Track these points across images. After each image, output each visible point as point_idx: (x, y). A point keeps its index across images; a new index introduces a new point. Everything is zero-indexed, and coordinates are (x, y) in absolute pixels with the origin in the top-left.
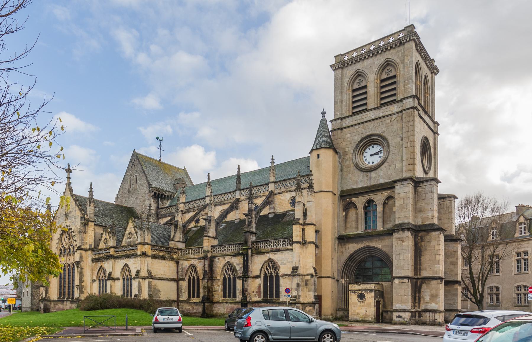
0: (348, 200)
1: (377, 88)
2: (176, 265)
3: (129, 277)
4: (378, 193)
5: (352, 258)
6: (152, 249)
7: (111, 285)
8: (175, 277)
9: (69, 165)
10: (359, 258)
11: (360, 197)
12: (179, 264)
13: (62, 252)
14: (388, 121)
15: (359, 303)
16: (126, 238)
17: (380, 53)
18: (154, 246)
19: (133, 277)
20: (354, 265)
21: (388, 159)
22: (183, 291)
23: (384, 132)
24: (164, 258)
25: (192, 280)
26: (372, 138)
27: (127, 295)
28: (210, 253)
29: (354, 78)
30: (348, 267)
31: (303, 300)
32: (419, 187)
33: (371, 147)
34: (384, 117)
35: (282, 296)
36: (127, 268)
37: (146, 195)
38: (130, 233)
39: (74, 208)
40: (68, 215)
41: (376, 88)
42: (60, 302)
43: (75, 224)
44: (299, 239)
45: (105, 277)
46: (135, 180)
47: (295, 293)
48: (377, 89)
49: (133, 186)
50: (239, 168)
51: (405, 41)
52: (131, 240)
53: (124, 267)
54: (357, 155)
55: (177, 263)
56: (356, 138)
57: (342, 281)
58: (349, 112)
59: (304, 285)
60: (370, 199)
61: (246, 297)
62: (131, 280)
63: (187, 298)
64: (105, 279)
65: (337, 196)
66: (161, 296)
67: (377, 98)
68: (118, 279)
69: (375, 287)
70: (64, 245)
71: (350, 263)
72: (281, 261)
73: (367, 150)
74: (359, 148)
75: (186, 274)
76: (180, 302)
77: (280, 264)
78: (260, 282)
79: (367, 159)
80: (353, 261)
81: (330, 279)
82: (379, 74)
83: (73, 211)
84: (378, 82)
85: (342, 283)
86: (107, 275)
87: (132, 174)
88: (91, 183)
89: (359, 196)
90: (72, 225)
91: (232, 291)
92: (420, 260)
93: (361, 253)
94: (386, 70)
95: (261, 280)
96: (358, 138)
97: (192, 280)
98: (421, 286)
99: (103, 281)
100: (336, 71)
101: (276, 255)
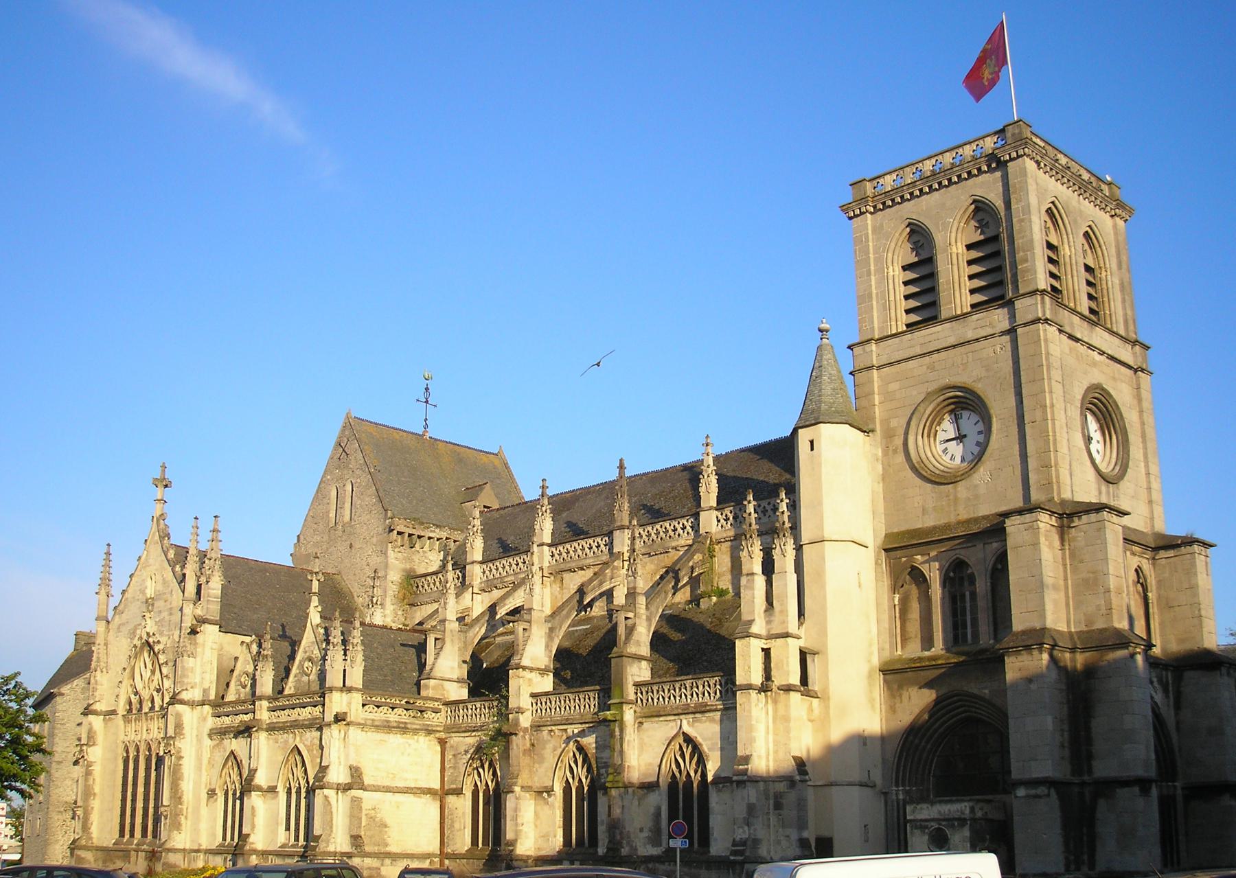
2: (439, 748)
13: (134, 707)
20: (929, 746)
24: (403, 728)
25: (481, 795)
31: (769, 852)
32: (1069, 527)
35: (716, 840)
40: (153, 605)
47: (744, 832)
56: (915, 393)
57: (897, 795)
59: (771, 807)
60: (957, 558)
66: (389, 841)
69: (972, 810)
70: (139, 686)
71: (917, 741)
81: (858, 787)
85: (898, 800)
95: (660, 795)
97: (481, 795)
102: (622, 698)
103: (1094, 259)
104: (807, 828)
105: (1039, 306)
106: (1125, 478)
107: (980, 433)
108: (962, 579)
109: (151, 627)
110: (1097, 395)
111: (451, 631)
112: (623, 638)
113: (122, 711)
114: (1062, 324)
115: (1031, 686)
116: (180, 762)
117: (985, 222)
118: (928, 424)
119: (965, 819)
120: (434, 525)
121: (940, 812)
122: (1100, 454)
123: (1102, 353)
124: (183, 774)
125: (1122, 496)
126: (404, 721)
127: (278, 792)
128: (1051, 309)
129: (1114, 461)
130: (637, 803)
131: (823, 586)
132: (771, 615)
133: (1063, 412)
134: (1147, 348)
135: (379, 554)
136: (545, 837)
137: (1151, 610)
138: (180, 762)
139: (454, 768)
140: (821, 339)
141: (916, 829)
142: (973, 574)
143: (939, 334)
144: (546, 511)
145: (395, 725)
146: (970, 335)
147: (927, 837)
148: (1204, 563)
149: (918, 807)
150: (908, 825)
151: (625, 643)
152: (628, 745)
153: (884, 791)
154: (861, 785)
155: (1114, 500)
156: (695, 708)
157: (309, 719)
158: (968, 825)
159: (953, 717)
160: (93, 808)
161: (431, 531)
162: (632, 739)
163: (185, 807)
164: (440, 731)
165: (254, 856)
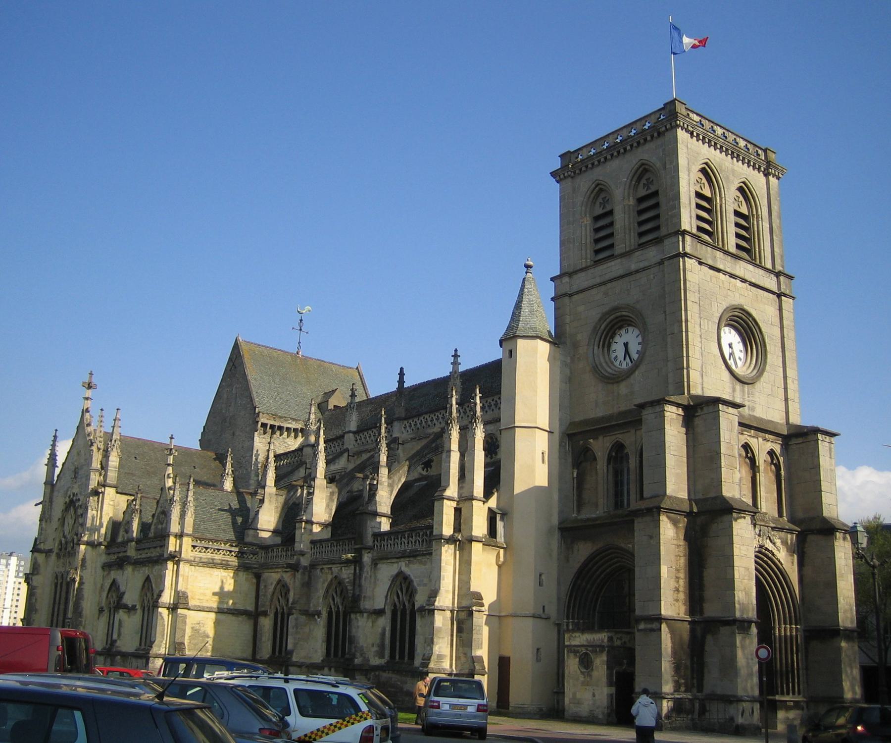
2: (255, 581)
8: (250, 607)
12: (262, 579)
15: (582, 678)
17: (585, 171)
20: (593, 589)
25: (399, 613)
26: (619, 314)
33: (623, 331)
34: (637, 272)
41: (627, 216)
48: (629, 217)
50: (402, 374)
51: (664, 129)
54: (596, 348)
55: (258, 577)
67: (630, 235)
69: (610, 639)
73: (617, 338)
78: (384, 622)
79: (617, 357)
84: (631, 203)
94: (644, 181)
96: (595, 314)
97: (399, 613)
98: (704, 638)
100: (561, 182)
102: (362, 544)
103: (748, 208)
104: (482, 648)
105: (681, 243)
106: (762, 379)
107: (639, 344)
109: (75, 491)
110: (736, 313)
111: (270, 494)
112: (366, 499)
113: (56, 551)
114: (700, 257)
115: (652, 541)
116: (82, 587)
117: (651, 180)
118: (603, 337)
119: (603, 647)
120: (291, 419)
122: (742, 361)
123: (744, 281)
124: (83, 595)
125: (757, 394)
126: (226, 559)
127: (137, 609)
128: (692, 246)
129: (753, 366)
130: (371, 625)
132: (463, 482)
134: (791, 278)
135: (249, 440)
136: (261, 525)
138: (82, 587)
140: (526, 273)
141: (571, 652)
143: (615, 268)
144: (353, 408)
145: (219, 562)
146: (633, 267)
147: (578, 659)
148: (828, 449)
149: (573, 635)
150: (566, 649)
151: (367, 503)
152: (365, 580)
153: (557, 622)
155: (748, 397)
156: (410, 552)
157: (157, 556)
158: (606, 652)
160: (34, 620)
161: (289, 423)
162: (368, 576)
163: (83, 620)
164: (255, 568)
165: (119, 657)
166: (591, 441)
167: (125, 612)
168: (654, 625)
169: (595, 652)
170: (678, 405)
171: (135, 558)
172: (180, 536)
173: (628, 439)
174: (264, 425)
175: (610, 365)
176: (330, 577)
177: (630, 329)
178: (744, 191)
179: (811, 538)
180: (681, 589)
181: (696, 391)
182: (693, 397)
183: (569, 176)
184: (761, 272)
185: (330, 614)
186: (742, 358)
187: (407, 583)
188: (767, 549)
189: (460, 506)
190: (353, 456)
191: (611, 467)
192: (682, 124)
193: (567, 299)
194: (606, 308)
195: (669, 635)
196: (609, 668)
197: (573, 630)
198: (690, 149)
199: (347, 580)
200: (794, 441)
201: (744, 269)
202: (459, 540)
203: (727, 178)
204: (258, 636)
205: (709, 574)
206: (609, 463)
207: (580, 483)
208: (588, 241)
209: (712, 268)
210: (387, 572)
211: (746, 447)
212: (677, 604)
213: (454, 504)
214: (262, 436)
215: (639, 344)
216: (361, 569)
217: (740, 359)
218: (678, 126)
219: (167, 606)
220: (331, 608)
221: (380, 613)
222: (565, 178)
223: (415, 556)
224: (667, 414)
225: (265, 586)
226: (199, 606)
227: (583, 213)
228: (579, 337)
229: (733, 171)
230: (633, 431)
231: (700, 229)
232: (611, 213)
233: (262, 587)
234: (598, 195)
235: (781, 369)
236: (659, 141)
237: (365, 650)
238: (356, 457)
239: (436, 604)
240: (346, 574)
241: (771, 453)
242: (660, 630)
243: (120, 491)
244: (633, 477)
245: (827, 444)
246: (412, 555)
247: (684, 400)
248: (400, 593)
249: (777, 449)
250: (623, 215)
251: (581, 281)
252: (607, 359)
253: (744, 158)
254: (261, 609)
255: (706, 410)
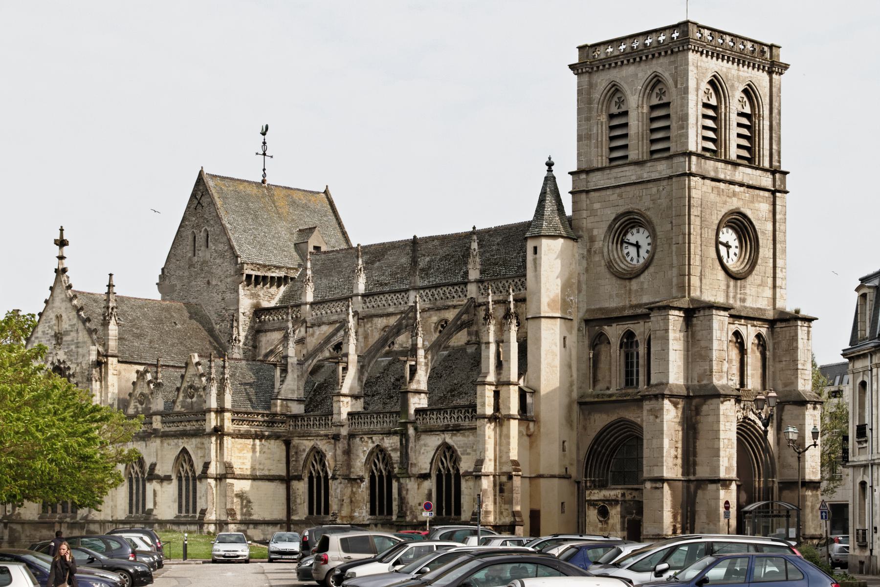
0: (597, 328)
1: (642, 121)
2: (284, 447)
3: (190, 474)
4: (640, 321)
5: (602, 440)
6: (233, 420)
7: (154, 491)
8: (283, 472)
9: (62, 230)
10: (614, 440)
11: (614, 325)
12: (292, 445)
14: (654, 190)
15: (600, 525)
16: (184, 397)
18: (238, 413)
19: (197, 475)
21: (655, 261)
22: (298, 501)
23: (649, 209)
25: (315, 480)
26: (632, 217)
27: (187, 511)
28: (346, 427)
29: (609, 94)
30: (596, 455)
33: (635, 231)
34: (649, 181)
36: (186, 458)
37: (229, 280)
38: (191, 387)
39: (74, 325)
40: (62, 339)
41: (640, 123)
42: (45, 525)
43: (77, 359)
44: (489, 411)
45: (143, 473)
46: (203, 241)
49: (200, 252)
52: (194, 399)
53: (179, 454)
54: (610, 244)
55: (287, 443)
58: (602, 159)
61: (405, 513)
62: (194, 479)
63: (305, 516)
64: (143, 478)
65: (575, 324)
68: (168, 478)
69: (623, 495)
72: (462, 447)
74: (613, 231)
75: (304, 466)
76: (293, 524)
77: (462, 454)
78: (430, 485)
79: (628, 253)
80: (600, 442)
82: (645, 96)
83: (72, 331)
86: (147, 467)
87: (198, 226)
88: (111, 275)
89: (614, 323)
90: (71, 361)
91: (385, 503)
92: (695, 447)
93: (615, 430)
96: (610, 214)
97: (315, 480)
98: (696, 493)
99: (137, 481)
101: (454, 438)
105: (687, 163)
106: (754, 273)
107: (649, 244)
108: (632, 343)
112: (408, 379)
121: (604, 496)
123: (741, 185)
125: (748, 286)
131: (539, 348)
133: (699, 237)
135: (232, 291)
136: (470, 468)
137: (767, 363)
139: (296, 461)
142: (637, 341)
146: (646, 176)
151: (409, 383)
154: (560, 477)
159: (625, 433)
161: (273, 272)
166: (606, 327)
167: (158, 482)
168: (659, 485)
169: (611, 505)
170: (680, 309)
171: (162, 430)
172: (221, 411)
173: (639, 329)
174: (249, 277)
175: (623, 260)
176: (371, 446)
177: (641, 230)
178: (749, 93)
179: (788, 408)
180: (680, 456)
181: (696, 293)
182: (693, 300)
183: (587, 72)
184: (759, 172)
185: (372, 478)
186: (737, 253)
187: (450, 452)
188: (749, 419)
189: (498, 389)
190: (363, 319)
191: (622, 351)
192: (693, 48)
193: (584, 196)
194: (621, 210)
195: (669, 492)
196: (623, 517)
197: (590, 487)
198: (700, 66)
199: (390, 449)
200: (779, 325)
201: (744, 174)
202: (499, 418)
203: (732, 86)
204: (292, 498)
205: (701, 444)
206: (621, 347)
207: (595, 362)
208: (604, 139)
209: (713, 180)
210: (433, 442)
211: (737, 334)
212: (676, 468)
213: (493, 388)
214: (246, 288)
215: (649, 244)
216: (407, 441)
217: (735, 254)
218: (689, 49)
219: (215, 476)
220: (373, 472)
221: (425, 477)
222: (583, 73)
223: (458, 431)
224: (670, 317)
225: (296, 453)
226: (241, 475)
227: (599, 111)
228: (595, 232)
229: (738, 77)
230: (642, 323)
231: (704, 149)
232: (625, 114)
233: (292, 453)
234: (614, 94)
235: (771, 261)
236: (672, 58)
237: (414, 508)
238: (365, 320)
239: (483, 471)
240: (391, 443)
241: (759, 336)
242: (663, 487)
243: (120, 359)
244: (641, 362)
245: (806, 329)
246: (456, 429)
247: (684, 303)
248: (443, 459)
249: (764, 331)
250: (636, 122)
251: (597, 180)
252: (620, 255)
253: (749, 63)
254: (293, 473)
255: (702, 313)
